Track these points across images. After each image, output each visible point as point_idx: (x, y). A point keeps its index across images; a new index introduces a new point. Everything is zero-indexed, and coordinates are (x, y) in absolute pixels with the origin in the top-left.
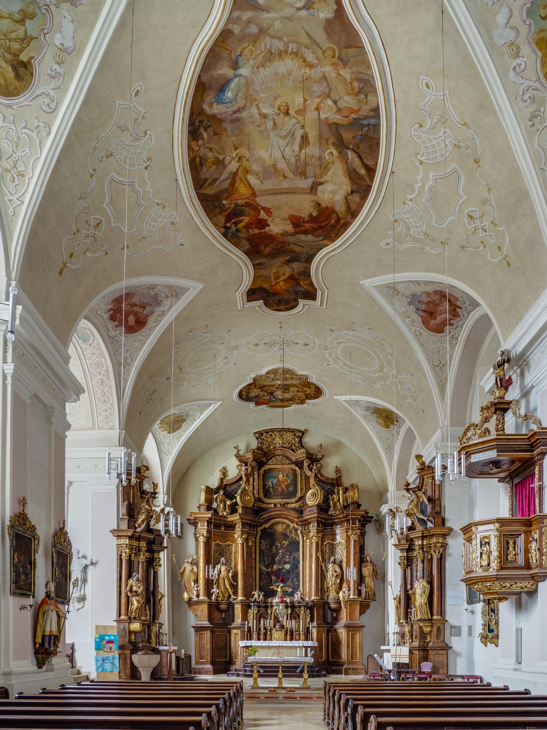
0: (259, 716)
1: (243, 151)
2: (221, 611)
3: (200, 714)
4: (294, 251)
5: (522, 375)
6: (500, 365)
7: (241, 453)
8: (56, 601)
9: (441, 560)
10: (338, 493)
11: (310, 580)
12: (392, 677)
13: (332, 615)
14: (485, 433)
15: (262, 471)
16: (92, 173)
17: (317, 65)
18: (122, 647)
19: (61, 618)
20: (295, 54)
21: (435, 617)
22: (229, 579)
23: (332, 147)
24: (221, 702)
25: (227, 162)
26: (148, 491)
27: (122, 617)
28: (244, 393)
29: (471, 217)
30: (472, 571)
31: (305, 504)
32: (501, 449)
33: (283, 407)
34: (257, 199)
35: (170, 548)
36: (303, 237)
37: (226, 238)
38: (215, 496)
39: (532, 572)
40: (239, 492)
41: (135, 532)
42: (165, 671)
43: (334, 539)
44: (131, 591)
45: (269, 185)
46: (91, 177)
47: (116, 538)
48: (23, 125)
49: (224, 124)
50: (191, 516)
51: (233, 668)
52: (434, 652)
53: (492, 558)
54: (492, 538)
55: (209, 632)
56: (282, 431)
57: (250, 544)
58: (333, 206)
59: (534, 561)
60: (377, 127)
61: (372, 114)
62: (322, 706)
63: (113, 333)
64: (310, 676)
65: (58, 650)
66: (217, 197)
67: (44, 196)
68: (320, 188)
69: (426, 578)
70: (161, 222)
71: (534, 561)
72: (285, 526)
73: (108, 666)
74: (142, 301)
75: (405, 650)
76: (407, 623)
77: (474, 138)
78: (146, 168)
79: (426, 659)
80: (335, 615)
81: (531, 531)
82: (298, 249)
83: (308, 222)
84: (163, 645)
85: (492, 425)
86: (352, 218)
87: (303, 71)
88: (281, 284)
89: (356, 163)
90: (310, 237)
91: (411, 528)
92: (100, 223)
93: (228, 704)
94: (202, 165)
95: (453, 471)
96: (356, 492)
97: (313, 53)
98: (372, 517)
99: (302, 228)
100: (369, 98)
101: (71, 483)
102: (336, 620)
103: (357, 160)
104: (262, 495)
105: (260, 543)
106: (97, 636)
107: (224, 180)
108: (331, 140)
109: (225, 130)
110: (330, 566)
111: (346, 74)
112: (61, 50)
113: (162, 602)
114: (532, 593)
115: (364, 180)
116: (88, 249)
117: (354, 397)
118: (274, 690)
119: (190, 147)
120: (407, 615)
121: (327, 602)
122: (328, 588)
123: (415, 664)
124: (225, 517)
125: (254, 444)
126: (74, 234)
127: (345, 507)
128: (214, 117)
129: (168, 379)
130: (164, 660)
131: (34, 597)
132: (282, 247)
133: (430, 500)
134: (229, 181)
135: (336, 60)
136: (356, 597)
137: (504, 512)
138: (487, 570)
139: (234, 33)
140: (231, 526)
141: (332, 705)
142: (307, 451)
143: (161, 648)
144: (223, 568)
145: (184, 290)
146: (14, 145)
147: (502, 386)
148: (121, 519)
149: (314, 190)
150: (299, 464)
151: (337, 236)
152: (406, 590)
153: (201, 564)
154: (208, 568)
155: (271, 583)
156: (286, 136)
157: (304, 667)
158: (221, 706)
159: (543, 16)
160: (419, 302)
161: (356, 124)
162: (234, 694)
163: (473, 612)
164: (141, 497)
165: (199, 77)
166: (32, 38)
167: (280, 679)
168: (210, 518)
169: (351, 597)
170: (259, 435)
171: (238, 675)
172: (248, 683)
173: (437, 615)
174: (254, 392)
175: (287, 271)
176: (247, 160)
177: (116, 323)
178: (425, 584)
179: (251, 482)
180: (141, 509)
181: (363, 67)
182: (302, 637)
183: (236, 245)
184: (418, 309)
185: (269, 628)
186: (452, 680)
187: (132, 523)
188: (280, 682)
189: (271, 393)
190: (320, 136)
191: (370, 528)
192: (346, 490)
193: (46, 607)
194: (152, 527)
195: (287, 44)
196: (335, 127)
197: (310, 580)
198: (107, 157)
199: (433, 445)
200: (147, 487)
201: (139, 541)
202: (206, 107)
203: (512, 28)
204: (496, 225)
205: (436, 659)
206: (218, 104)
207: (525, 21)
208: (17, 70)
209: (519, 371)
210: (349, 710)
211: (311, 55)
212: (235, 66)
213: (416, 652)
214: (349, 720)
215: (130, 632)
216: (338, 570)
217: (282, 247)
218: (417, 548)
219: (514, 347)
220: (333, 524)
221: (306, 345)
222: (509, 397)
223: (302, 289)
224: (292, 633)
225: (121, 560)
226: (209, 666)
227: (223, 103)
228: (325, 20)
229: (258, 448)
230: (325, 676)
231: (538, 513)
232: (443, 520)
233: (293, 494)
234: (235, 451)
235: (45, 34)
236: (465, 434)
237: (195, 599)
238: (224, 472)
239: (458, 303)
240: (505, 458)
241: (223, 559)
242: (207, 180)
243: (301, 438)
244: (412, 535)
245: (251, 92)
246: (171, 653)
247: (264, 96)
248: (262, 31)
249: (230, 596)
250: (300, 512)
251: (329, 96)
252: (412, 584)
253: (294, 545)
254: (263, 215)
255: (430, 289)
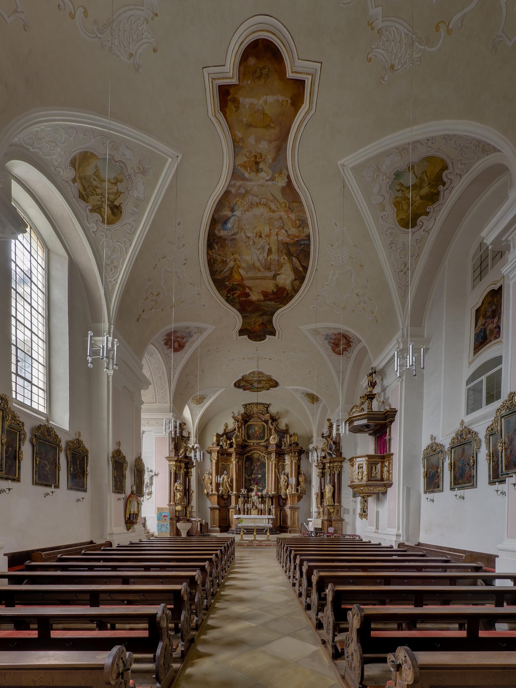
0: (244, 555)
1: (237, 256)
2: (224, 499)
3: (212, 554)
4: (264, 310)
5: (382, 379)
6: (371, 375)
7: (235, 415)
8: (136, 495)
9: (340, 474)
10: (287, 438)
11: (272, 483)
12: (313, 535)
13: (283, 502)
14: (361, 410)
15: (246, 425)
16: (155, 266)
17: (277, 211)
18: (171, 519)
19: (139, 504)
20: (265, 205)
21: (336, 504)
22: (228, 483)
23: (284, 255)
24: (223, 548)
25: (228, 261)
26: (185, 436)
27: (172, 503)
28: (237, 384)
29: (357, 295)
30: (353, 482)
31: (269, 443)
32: (369, 419)
33: (258, 391)
34: (244, 282)
35: (197, 466)
36: (269, 302)
37: (227, 302)
38: (221, 438)
39: (384, 482)
40: (234, 436)
41: (178, 458)
42: (194, 531)
43: (284, 462)
44: (176, 489)
45: (251, 274)
46: (154, 269)
47: (168, 461)
48: (117, 240)
49: (226, 241)
50: (208, 449)
51: (231, 529)
52: (335, 522)
53: (364, 475)
54: (364, 464)
55: (218, 510)
56: (257, 404)
57: (240, 464)
58: (285, 287)
59: (385, 477)
60: (309, 245)
61: (306, 238)
62: (276, 550)
63: (166, 352)
64: (270, 534)
65: (138, 521)
66: (223, 280)
67: (128, 279)
68: (278, 277)
69: (331, 484)
70: (192, 293)
71: (385, 477)
72: (258, 455)
73: (164, 529)
74: (182, 335)
75: (319, 521)
76: (321, 507)
77: (360, 253)
78: (184, 264)
79: (331, 526)
80: (284, 502)
81: (384, 462)
82: (266, 309)
83: (272, 294)
84: (193, 518)
85: (365, 406)
86: (295, 293)
87: (269, 214)
88: (257, 327)
89: (298, 264)
90: (273, 303)
91: (324, 457)
92: (159, 294)
93: (227, 549)
94: (214, 263)
95: (342, 432)
96: (296, 437)
97: (275, 205)
98: (304, 451)
99: (268, 298)
100: (305, 230)
101: (144, 432)
102: (285, 504)
103: (298, 262)
104: (246, 438)
105: (245, 463)
106: (158, 513)
107: (226, 271)
108: (284, 252)
109: (227, 244)
110: (282, 476)
111: (292, 216)
112: (137, 200)
113: (193, 495)
114: (385, 493)
115: (302, 273)
116: (152, 308)
117: (295, 387)
118: (251, 541)
119: (208, 253)
120: (322, 502)
121: (281, 495)
122: (281, 487)
123: (325, 528)
124: (227, 450)
125: (242, 411)
126: (145, 299)
127: (290, 445)
128: (221, 237)
129: (196, 376)
130: (194, 525)
131: (125, 494)
132: (257, 308)
133: (334, 443)
134: (229, 272)
135: (287, 208)
136: (296, 492)
137: (372, 452)
138: (361, 481)
139: (232, 193)
140: (230, 455)
141: (280, 549)
142: (271, 415)
143: (192, 519)
144: (225, 477)
145: (205, 329)
146: (112, 251)
147: (371, 386)
148: (171, 451)
149: (275, 278)
150: (266, 422)
151: (287, 302)
152: (321, 490)
153: (214, 475)
154: (217, 477)
155: (251, 485)
156: (260, 249)
157: (267, 529)
158: (223, 550)
159: (398, 189)
160: (330, 338)
161: (297, 243)
162: (230, 544)
163: (355, 502)
164: (182, 439)
165: (213, 216)
166: (121, 193)
167: (255, 536)
168: (219, 450)
169: (293, 492)
170: (245, 406)
171: (233, 533)
172: (237, 538)
173: (337, 503)
174: (243, 384)
175: (260, 320)
176: (239, 261)
177: (168, 347)
178: (331, 487)
179: (241, 431)
180: (181, 446)
181: (302, 213)
182: (267, 513)
183: (233, 306)
184: (330, 342)
185: (249, 508)
186: (344, 537)
187: (176, 454)
188: (255, 537)
189: (252, 384)
190: (278, 249)
191: (303, 456)
192: (291, 436)
193: (131, 499)
194: (187, 455)
195: (260, 199)
196: (286, 245)
197: (272, 483)
198: (163, 258)
199: (336, 414)
200: (185, 434)
201: (181, 463)
202: (216, 232)
203: (381, 195)
204: (371, 300)
205: (336, 526)
206: (223, 230)
207: (388, 192)
208: (113, 210)
209: (381, 378)
210: (288, 552)
211: (274, 205)
212: (233, 210)
213: (326, 522)
214: (288, 558)
215: (176, 511)
216: (286, 478)
217: (257, 308)
218: (327, 468)
219: (378, 365)
220: (284, 454)
221: (270, 359)
222: (374, 392)
223: (268, 330)
224: (262, 511)
225: (171, 473)
226: (218, 529)
227: (226, 230)
228: (281, 187)
229: (245, 413)
230: (279, 534)
231: (388, 452)
232: (341, 453)
233: (263, 438)
234: (232, 415)
235: (128, 191)
236: (351, 410)
237: (211, 493)
238: (226, 426)
239: (351, 340)
240: (372, 423)
241: (225, 472)
242: (217, 271)
243: (267, 408)
244: (325, 461)
245: (241, 225)
246: (197, 522)
247: (248, 227)
248: (247, 192)
249: (229, 491)
250: (267, 447)
251: (283, 228)
252: (324, 487)
253: (263, 465)
254: (247, 290)
255: (336, 332)
